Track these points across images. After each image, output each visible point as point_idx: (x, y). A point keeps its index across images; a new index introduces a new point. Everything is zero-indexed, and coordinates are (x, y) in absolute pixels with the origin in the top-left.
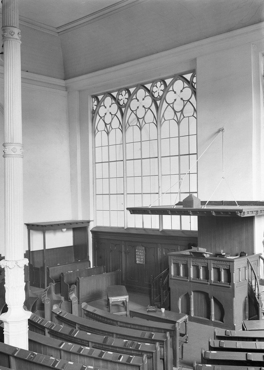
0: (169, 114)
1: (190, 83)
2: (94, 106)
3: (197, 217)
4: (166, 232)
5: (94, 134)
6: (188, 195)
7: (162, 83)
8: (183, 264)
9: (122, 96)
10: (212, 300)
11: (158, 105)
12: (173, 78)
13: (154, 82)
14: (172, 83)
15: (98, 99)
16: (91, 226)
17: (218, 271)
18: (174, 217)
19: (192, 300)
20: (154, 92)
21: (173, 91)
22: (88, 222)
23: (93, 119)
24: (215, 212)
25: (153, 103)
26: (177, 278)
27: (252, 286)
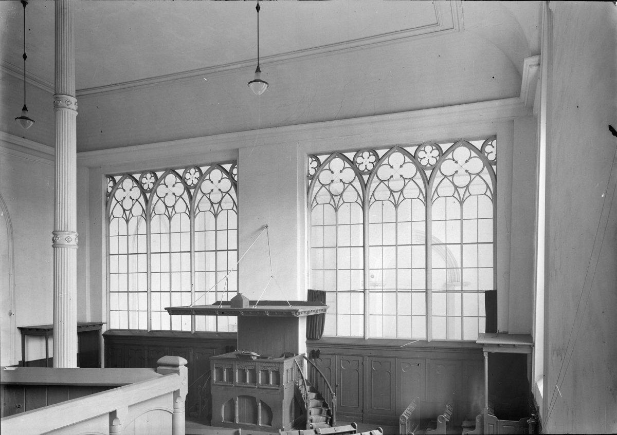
0: (446, 189)
1: (229, 174)
2: (109, 188)
3: (236, 317)
4: (114, 331)
5: (108, 221)
6: (236, 294)
7: (152, 175)
8: (263, 370)
9: (147, 179)
10: (260, 404)
11: (148, 198)
12: (209, 167)
13: (144, 173)
14: (209, 172)
15: (114, 180)
16: (104, 329)
17: (266, 373)
18: (184, 317)
19: (237, 406)
20: (187, 179)
21: (122, 188)
22: (101, 324)
23: (107, 204)
24: (244, 312)
25: (186, 191)
26: (242, 385)
27: (298, 386)
